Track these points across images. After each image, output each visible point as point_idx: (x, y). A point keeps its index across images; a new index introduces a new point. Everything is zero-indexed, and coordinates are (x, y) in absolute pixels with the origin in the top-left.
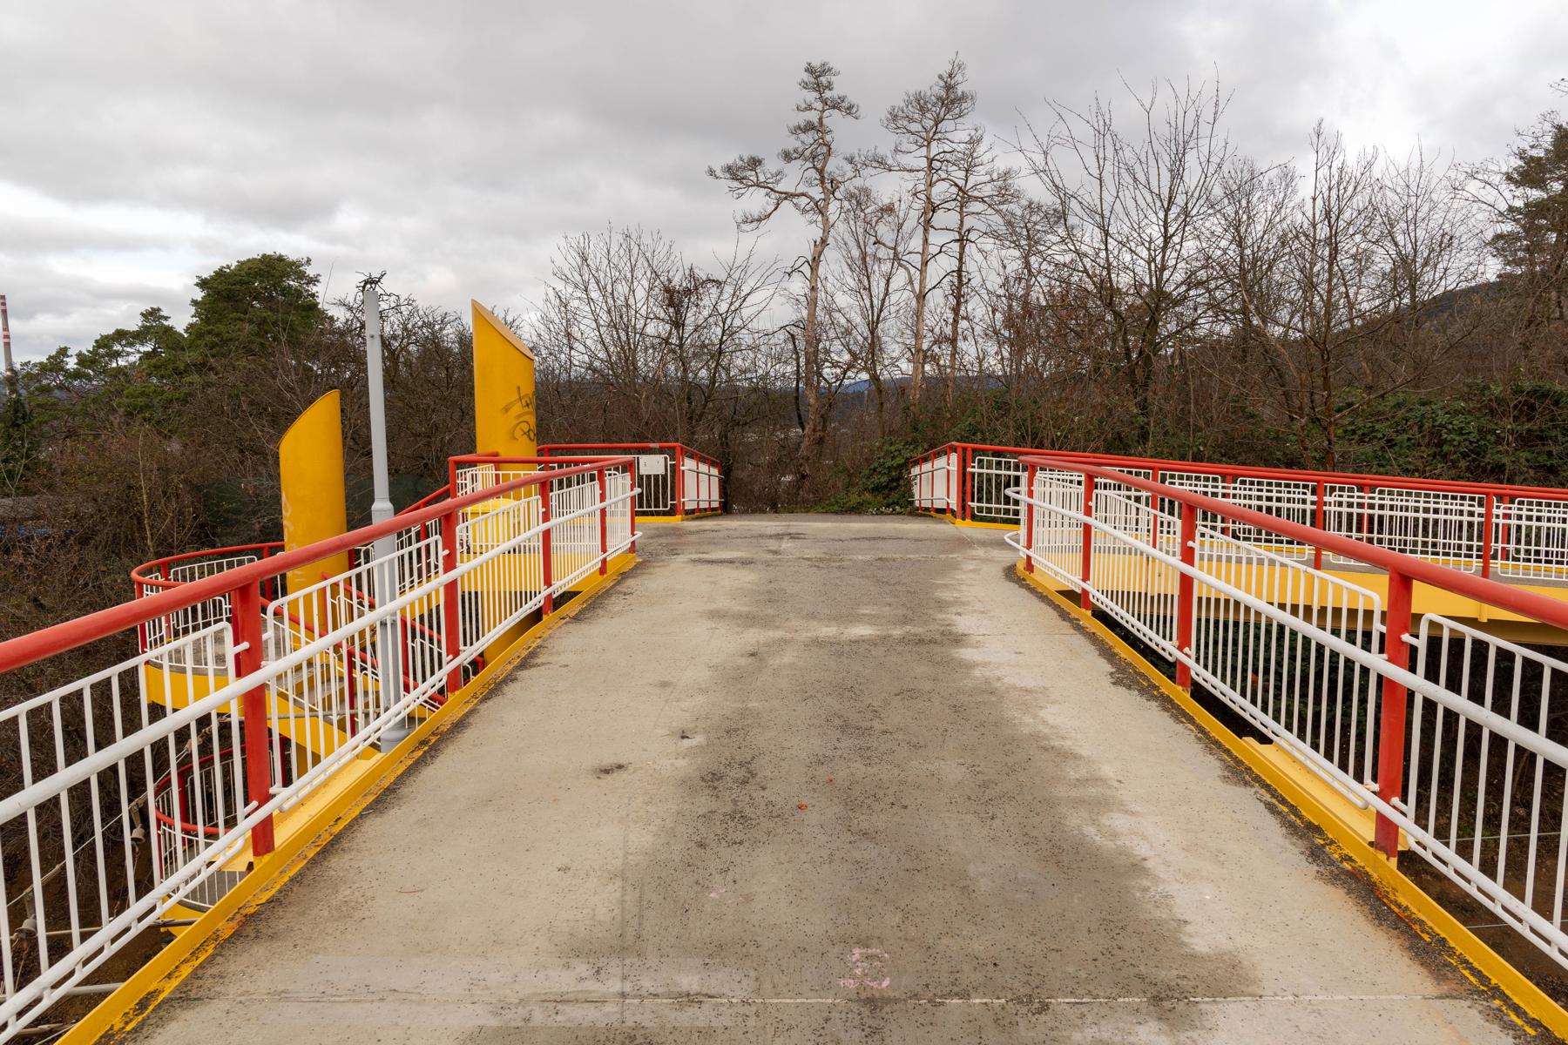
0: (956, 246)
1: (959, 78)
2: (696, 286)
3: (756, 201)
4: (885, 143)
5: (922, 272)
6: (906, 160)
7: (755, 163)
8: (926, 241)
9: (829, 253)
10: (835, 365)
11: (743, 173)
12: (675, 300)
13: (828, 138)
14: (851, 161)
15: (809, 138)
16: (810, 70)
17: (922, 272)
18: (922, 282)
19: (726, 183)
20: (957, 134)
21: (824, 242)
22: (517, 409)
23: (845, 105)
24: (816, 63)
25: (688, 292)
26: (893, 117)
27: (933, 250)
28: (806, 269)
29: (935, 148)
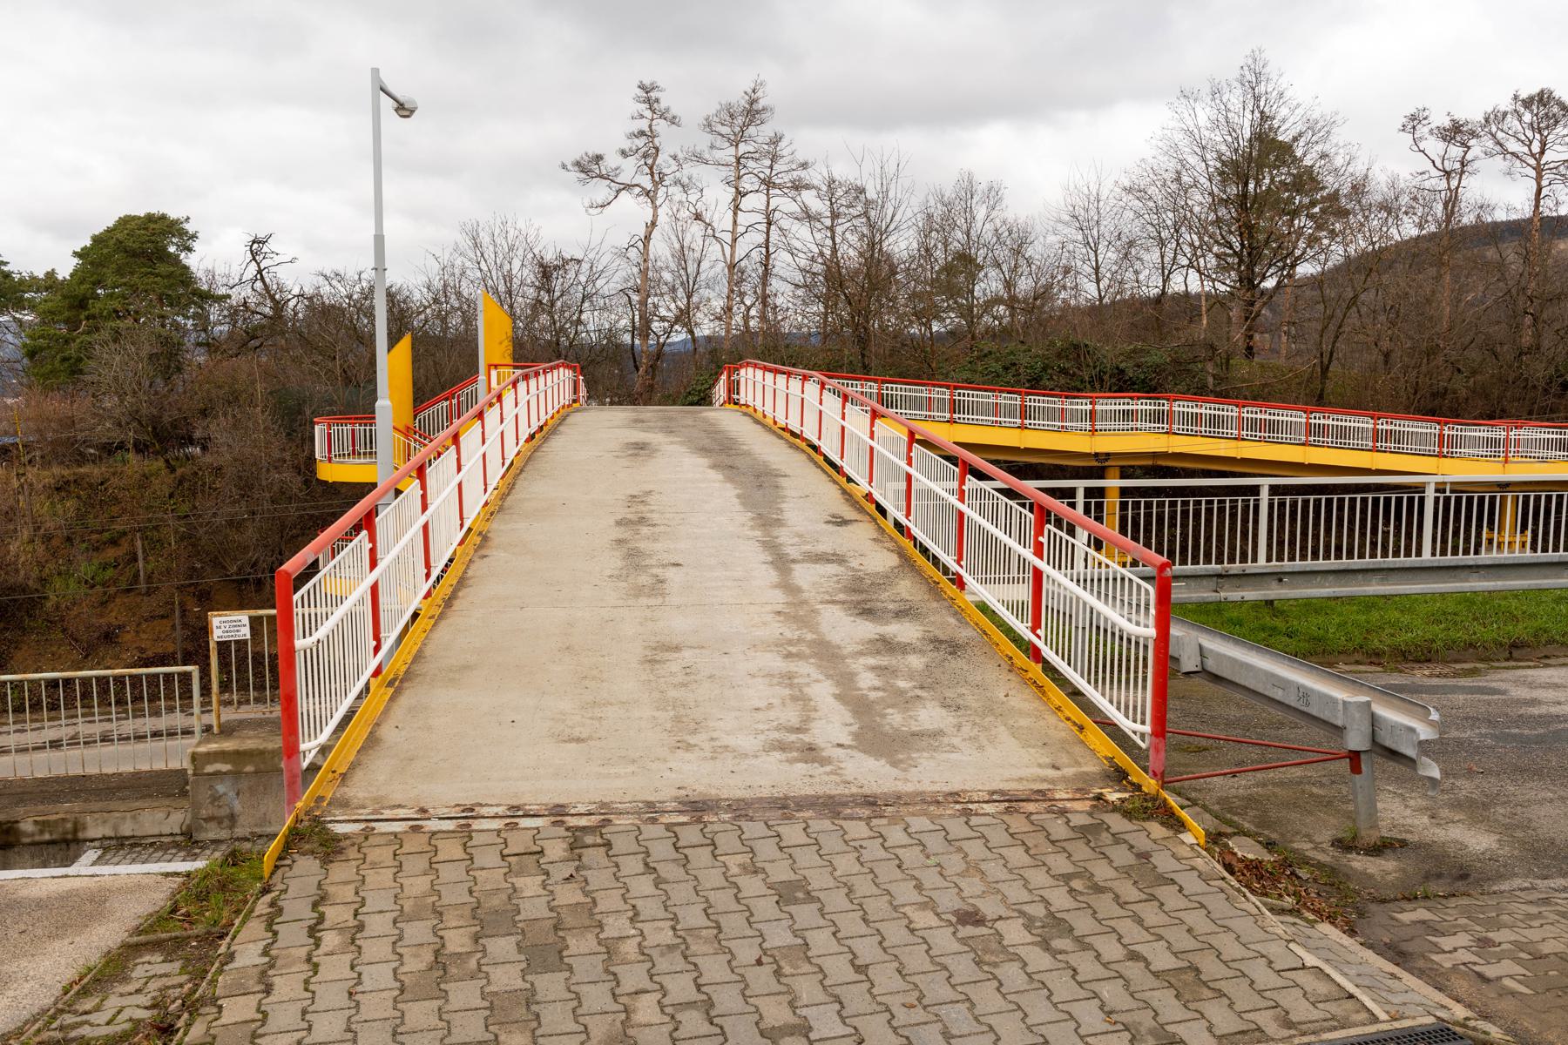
0: (763, 227)
1: (759, 94)
2: (564, 263)
3: (601, 191)
4: (702, 141)
5: (732, 247)
6: (718, 155)
7: (598, 158)
8: (735, 222)
9: (656, 234)
10: (663, 319)
11: (589, 167)
12: (546, 272)
13: (656, 141)
14: (675, 158)
15: (640, 142)
16: (642, 87)
17: (732, 247)
18: (732, 255)
19: (575, 175)
20: (761, 133)
21: (654, 224)
22: (506, 343)
23: (669, 116)
24: (647, 82)
25: (556, 268)
26: (709, 125)
27: (741, 229)
28: (640, 245)
29: (743, 148)
